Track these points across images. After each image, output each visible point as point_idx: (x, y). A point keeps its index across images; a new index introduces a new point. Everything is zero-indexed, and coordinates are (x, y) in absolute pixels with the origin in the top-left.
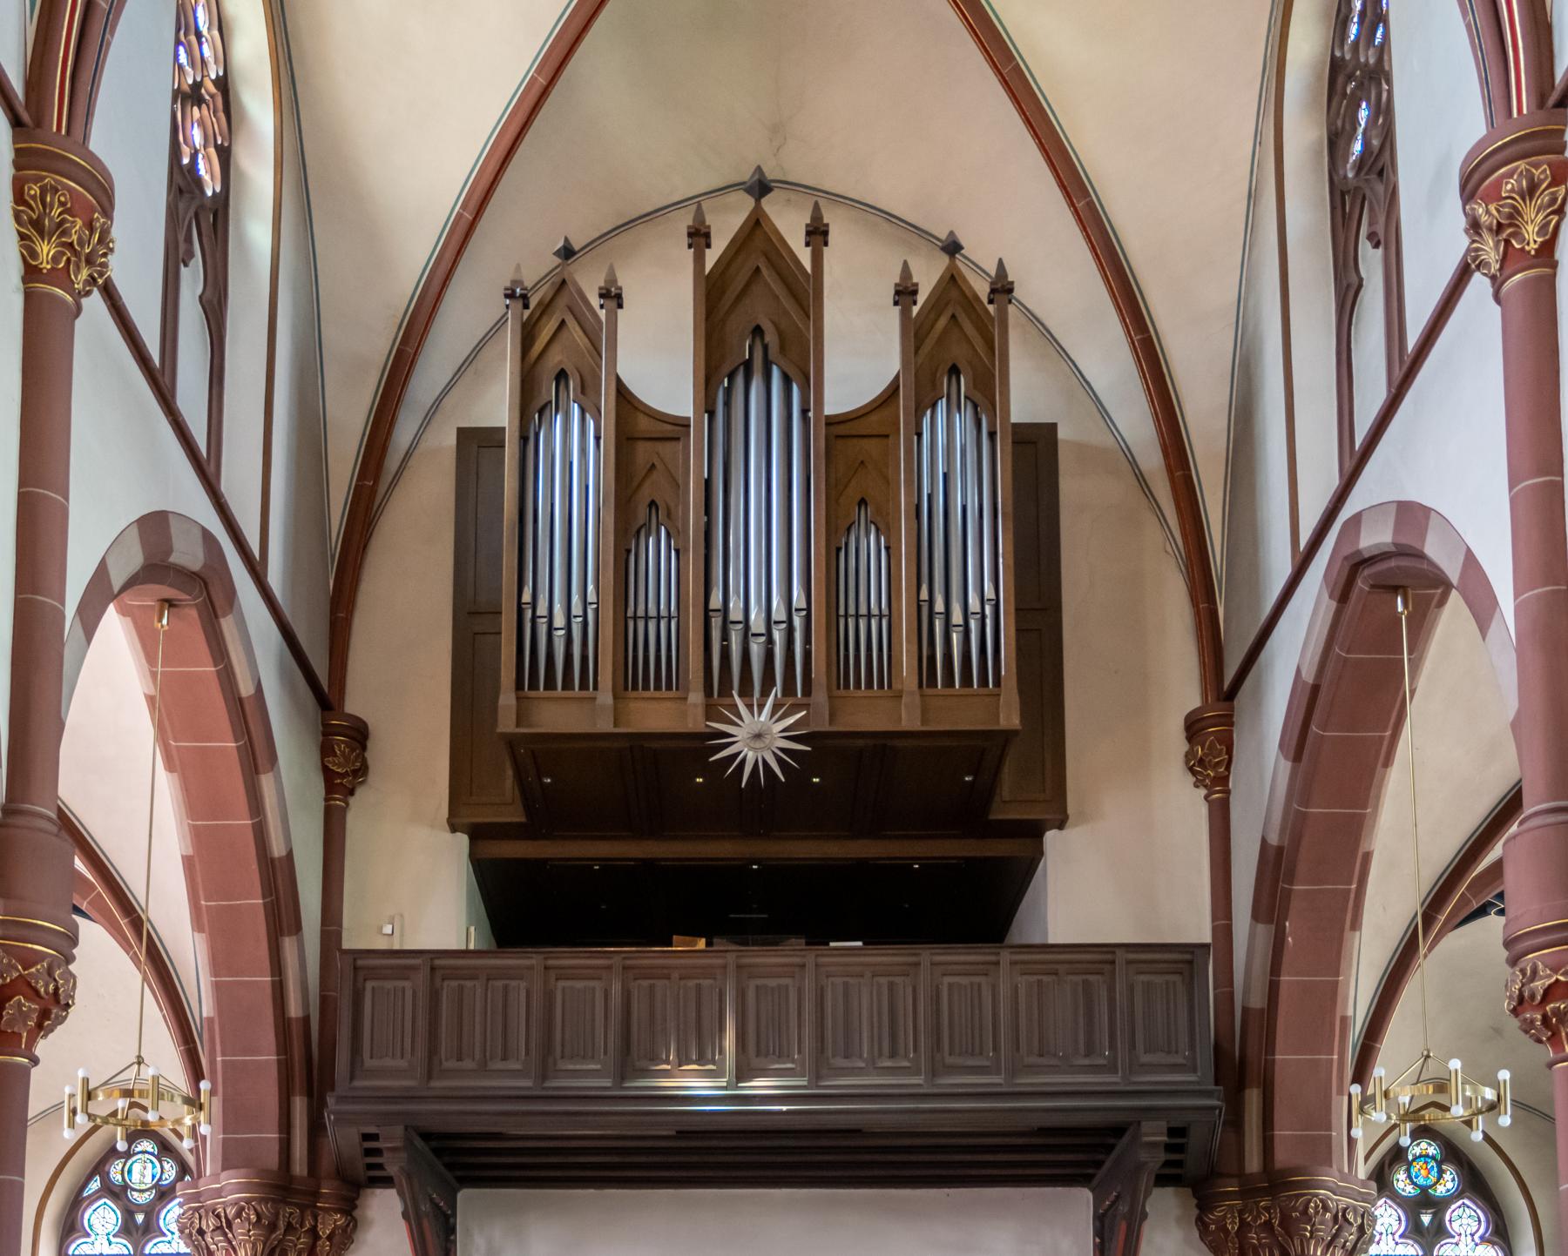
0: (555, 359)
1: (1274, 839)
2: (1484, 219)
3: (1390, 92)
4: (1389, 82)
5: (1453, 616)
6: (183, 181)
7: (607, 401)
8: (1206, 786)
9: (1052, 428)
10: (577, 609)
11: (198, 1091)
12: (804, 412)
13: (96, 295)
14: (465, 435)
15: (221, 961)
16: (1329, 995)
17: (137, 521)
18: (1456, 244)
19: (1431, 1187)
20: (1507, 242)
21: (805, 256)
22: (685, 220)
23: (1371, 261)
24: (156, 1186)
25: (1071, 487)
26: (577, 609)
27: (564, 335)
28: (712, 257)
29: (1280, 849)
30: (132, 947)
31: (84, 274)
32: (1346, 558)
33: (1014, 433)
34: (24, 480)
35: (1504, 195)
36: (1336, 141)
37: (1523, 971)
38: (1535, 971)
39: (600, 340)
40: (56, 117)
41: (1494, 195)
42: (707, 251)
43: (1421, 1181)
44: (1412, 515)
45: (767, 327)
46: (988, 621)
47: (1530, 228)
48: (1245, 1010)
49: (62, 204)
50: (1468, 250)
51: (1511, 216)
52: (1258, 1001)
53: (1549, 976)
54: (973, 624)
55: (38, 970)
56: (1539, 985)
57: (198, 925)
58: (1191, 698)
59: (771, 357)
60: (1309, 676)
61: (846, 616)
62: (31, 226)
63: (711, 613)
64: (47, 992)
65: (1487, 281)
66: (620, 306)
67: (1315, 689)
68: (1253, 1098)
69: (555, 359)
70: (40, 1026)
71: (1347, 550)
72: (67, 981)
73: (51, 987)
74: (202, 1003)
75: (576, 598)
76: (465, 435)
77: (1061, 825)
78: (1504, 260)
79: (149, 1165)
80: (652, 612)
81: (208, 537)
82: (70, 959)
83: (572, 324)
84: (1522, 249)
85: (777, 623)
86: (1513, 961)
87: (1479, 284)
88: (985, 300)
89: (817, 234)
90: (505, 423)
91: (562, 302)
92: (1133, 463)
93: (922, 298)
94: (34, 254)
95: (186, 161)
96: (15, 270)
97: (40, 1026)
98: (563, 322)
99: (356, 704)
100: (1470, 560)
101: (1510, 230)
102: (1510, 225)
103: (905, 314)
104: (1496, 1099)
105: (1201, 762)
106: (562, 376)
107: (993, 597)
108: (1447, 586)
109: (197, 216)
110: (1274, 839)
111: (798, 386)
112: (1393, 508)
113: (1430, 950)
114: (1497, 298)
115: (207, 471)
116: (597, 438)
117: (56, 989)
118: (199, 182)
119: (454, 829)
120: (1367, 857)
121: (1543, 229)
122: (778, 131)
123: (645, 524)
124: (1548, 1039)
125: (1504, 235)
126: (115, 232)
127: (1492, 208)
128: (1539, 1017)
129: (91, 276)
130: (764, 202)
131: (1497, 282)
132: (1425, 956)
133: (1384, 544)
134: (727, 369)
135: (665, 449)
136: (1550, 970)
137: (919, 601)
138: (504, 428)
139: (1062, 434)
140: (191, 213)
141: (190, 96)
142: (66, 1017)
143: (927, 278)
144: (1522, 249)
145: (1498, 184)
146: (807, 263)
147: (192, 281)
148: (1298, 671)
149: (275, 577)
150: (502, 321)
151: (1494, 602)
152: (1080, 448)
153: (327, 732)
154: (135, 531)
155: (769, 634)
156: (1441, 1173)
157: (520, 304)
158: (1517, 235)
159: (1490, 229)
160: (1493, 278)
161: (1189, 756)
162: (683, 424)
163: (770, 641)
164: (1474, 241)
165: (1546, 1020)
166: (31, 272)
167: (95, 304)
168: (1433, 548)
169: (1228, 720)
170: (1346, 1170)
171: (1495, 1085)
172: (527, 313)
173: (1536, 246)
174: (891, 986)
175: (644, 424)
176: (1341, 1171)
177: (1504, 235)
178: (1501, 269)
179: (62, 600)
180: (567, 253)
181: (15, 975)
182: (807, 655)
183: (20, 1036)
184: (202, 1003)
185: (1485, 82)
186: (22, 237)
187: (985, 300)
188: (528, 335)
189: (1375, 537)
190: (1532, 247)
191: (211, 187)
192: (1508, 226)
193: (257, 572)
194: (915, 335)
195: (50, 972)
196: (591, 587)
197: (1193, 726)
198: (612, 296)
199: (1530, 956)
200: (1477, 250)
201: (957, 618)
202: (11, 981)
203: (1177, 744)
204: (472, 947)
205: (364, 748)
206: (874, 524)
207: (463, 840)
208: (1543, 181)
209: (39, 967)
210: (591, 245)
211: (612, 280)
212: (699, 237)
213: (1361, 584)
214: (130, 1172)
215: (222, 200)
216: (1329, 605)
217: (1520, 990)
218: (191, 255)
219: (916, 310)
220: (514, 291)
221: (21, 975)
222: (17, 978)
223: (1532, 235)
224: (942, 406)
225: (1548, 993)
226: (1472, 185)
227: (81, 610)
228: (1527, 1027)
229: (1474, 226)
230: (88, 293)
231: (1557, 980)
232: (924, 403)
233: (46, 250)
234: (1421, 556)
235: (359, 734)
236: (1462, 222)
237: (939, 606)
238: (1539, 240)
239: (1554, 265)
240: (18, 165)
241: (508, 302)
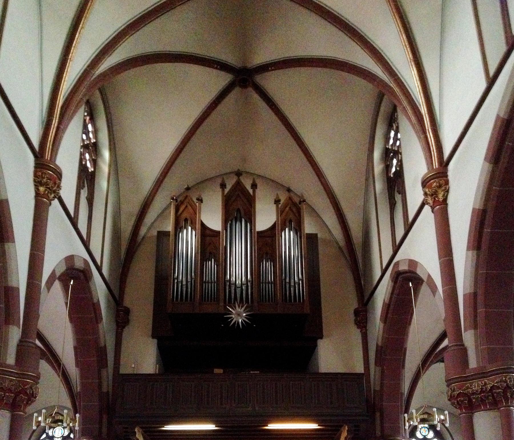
0: (185, 215)
1: (380, 344)
2: (428, 193)
3: (401, 157)
4: (401, 154)
5: (424, 289)
6: (83, 168)
7: (198, 226)
8: (361, 328)
9: (316, 235)
10: (189, 280)
11: (75, 417)
12: (251, 230)
13: (56, 200)
14: (159, 232)
15: (83, 376)
16: (398, 386)
17: (65, 258)
18: (420, 198)
19: (426, 435)
20: (435, 199)
21: (251, 191)
22: (219, 181)
23: (398, 198)
24: (62, 436)
25: (321, 249)
26: (189, 280)
27: (187, 210)
28: (227, 191)
29: (382, 347)
30: (57, 371)
31: (53, 195)
32: (396, 272)
33: (307, 236)
34: (32, 250)
35: (433, 187)
36: (388, 167)
37: (451, 389)
38: (454, 389)
39: (195, 212)
40: (48, 155)
41: (430, 187)
42: (225, 189)
43: (424, 434)
44: (413, 263)
45: (241, 208)
46: (301, 285)
47: (440, 195)
48: (374, 390)
49: (47, 177)
50: (424, 200)
51: (435, 192)
52: (378, 388)
53: (458, 391)
54: (296, 286)
55: (28, 387)
56: (456, 393)
57: (77, 365)
58: (355, 305)
59: (242, 216)
60: (387, 301)
61: (263, 283)
62: (38, 183)
63: (226, 282)
64: (30, 393)
65: (430, 207)
66: (202, 202)
67: (389, 305)
68: (378, 414)
69: (185, 215)
70: (27, 403)
71: (396, 270)
72: (36, 390)
73: (31, 392)
74: (78, 388)
75: (189, 277)
76: (159, 232)
77: (321, 338)
78: (434, 202)
79: (60, 430)
80: (210, 281)
81: (85, 261)
82: (37, 383)
83: (189, 207)
84: (438, 200)
85: (244, 284)
86: (448, 386)
87: (427, 209)
88: (298, 203)
89: (254, 186)
90: (171, 230)
91: (187, 200)
92: (337, 243)
93: (281, 202)
94: (38, 189)
95: (84, 163)
96: (33, 194)
97: (27, 403)
98: (186, 206)
99: (127, 303)
100: (429, 276)
101: (435, 196)
102: (435, 194)
103: (277, 206)
104: (445, 419)
105: (359, 322)
106: (186, 220)
107: (302, 278)
108: (423, 281)
109: (86, 177)
110: (380, 344)
111: (249, 223)
112: (408, 260)
113: (424, 374)
114: (433, 212)
115: (86, 244)
116: (195, 236)
117: (33, 392)
118: (87, 168)
119: (153, 337)
120: (406, 349)
121: (444, 195)
122: (244, 160)
123: (208, 258)
124: (459, 408)
125: (433, 197)
126: (62, 185)
127: (430, 190)
128: (456, 402)
129: (55, 196)
130: (241, 178)
131: (433, 208)
132: (423, 376)
133: (406, 270)
134: (230, 218)
135: (213, 239)
136: (459, 389)
137: (282, 279)
138: (170, 232)
139: (319, 236)
140: (85, 176)
141: (85, 147)
142: (35, 401)
143: (283, 199)
144: (438, 200)
145: (431, 184)
146: (252, 194)
147: (84, 194)
148: (384, 300)
149: (105, 271)
150: (170, 204)
151: (436, 288)
152: (324, 241)
153: (118, 311)
154: (64, 261)
155: (242, 286)
156: (429, 432)
157: (175, 201)
158: (437, 197)
159: (430, 195)
160: (431, 207)
161: (355, 321)
162: (218, 233)
163: (242, 289)
164: (426, 198)
165: (458, 402)
166: (38, 195)
167: (56, 202)
168: (419, 272)
169: (366, 311)
170: (404, 435)
171: (444, 415)
172: (177, 203)
173: (442, 200)
174: (276, 384)
175: (208, 232)
176: (403, 436)
177: (433, 197)
178: (433, 205)
179: (41, 281)
180: (188, 189)
181: (21, 389)
182: (252, 293)
183: (22, 406)
184: (78, 388)
185: (426, 159)
186: (35, 185)
187: (298, 203)
188: (177, 210)
189: (403, 267)
190: (441, 200)
191: (91, 169)
192: (434, 195)
193: (99, 269)
194: (280, 212)
195: (31, 388)
196: (193, 274)
197: (357, 313)
198: (200, 200)
199: (453, 385)
200: (427, 200)
201: (292, 284)
202: (19, 390)
203: (352, 317)
204: (157, 372)
205: (128, 315)
206: (270, 259)
207: (155, 341)
208: (442, 184)
209: (28, 386)
210: (193, 186)
211: (200, 196)
212: (223, 186)
213: (400, 279)
214: (55, 432)
215: (93, 174)
216: (391, 284)
217: (451, 394)
218: (84, 186)
219: (280, 205)
220: (173, 198)
221: (22, 389)
222: (21, 390)
223: (441, 197)
224: (287, 230)
225: (459, 395)
226: (425, 183)
227: (47, 282)
228: (453, 404)
229: (426, 194)
230: (54, 200)
231: (461, 392)
232: (283, 229)
233: (42, 189)
234: (416, 273)
235: (127, 311)
236: (422, 193)
237: (288, 280)
238: (443, 198)
239: (447, 204)
240: (36, 167)
241: (172, 200)
